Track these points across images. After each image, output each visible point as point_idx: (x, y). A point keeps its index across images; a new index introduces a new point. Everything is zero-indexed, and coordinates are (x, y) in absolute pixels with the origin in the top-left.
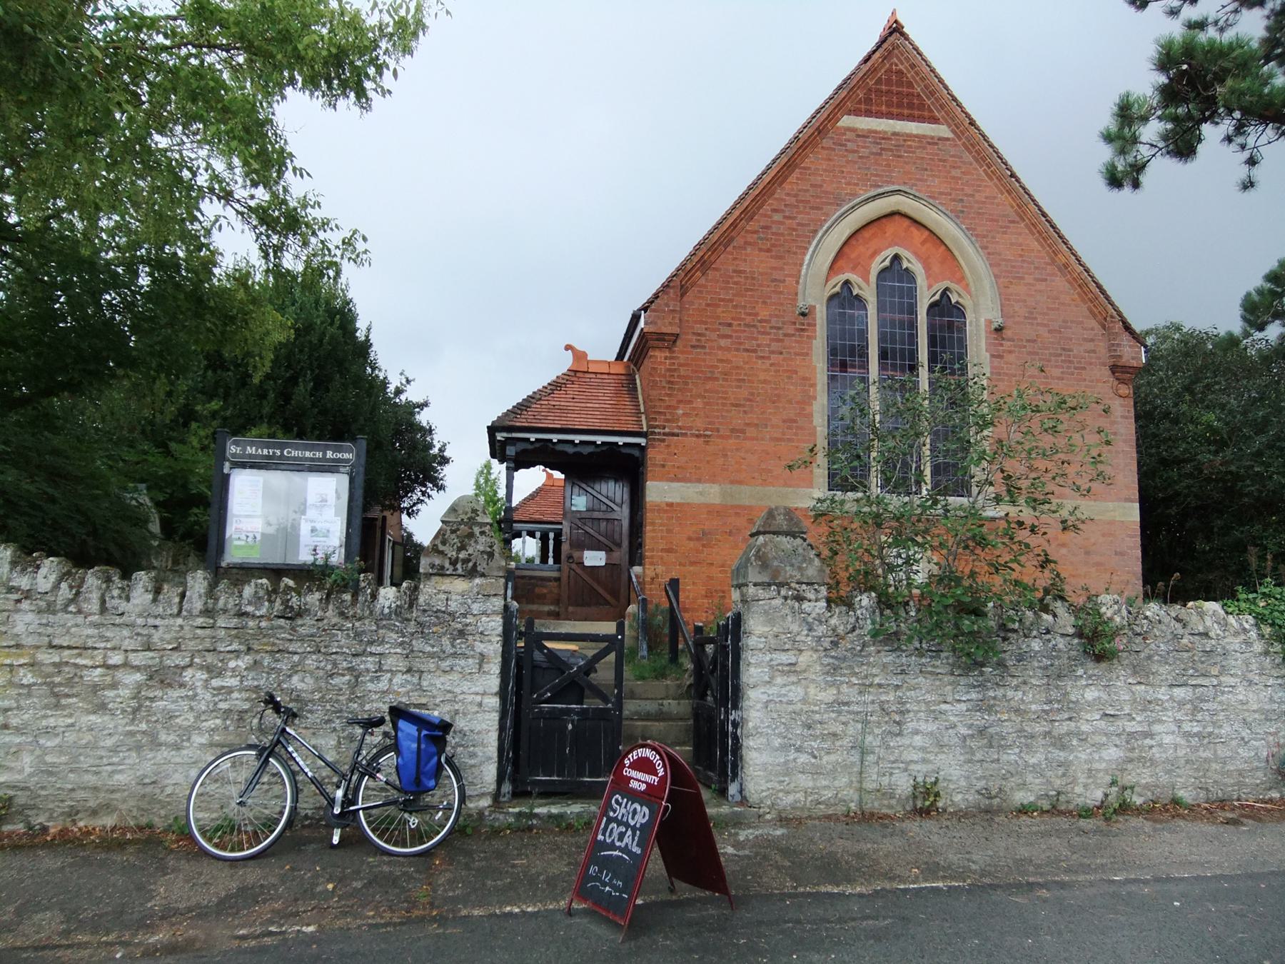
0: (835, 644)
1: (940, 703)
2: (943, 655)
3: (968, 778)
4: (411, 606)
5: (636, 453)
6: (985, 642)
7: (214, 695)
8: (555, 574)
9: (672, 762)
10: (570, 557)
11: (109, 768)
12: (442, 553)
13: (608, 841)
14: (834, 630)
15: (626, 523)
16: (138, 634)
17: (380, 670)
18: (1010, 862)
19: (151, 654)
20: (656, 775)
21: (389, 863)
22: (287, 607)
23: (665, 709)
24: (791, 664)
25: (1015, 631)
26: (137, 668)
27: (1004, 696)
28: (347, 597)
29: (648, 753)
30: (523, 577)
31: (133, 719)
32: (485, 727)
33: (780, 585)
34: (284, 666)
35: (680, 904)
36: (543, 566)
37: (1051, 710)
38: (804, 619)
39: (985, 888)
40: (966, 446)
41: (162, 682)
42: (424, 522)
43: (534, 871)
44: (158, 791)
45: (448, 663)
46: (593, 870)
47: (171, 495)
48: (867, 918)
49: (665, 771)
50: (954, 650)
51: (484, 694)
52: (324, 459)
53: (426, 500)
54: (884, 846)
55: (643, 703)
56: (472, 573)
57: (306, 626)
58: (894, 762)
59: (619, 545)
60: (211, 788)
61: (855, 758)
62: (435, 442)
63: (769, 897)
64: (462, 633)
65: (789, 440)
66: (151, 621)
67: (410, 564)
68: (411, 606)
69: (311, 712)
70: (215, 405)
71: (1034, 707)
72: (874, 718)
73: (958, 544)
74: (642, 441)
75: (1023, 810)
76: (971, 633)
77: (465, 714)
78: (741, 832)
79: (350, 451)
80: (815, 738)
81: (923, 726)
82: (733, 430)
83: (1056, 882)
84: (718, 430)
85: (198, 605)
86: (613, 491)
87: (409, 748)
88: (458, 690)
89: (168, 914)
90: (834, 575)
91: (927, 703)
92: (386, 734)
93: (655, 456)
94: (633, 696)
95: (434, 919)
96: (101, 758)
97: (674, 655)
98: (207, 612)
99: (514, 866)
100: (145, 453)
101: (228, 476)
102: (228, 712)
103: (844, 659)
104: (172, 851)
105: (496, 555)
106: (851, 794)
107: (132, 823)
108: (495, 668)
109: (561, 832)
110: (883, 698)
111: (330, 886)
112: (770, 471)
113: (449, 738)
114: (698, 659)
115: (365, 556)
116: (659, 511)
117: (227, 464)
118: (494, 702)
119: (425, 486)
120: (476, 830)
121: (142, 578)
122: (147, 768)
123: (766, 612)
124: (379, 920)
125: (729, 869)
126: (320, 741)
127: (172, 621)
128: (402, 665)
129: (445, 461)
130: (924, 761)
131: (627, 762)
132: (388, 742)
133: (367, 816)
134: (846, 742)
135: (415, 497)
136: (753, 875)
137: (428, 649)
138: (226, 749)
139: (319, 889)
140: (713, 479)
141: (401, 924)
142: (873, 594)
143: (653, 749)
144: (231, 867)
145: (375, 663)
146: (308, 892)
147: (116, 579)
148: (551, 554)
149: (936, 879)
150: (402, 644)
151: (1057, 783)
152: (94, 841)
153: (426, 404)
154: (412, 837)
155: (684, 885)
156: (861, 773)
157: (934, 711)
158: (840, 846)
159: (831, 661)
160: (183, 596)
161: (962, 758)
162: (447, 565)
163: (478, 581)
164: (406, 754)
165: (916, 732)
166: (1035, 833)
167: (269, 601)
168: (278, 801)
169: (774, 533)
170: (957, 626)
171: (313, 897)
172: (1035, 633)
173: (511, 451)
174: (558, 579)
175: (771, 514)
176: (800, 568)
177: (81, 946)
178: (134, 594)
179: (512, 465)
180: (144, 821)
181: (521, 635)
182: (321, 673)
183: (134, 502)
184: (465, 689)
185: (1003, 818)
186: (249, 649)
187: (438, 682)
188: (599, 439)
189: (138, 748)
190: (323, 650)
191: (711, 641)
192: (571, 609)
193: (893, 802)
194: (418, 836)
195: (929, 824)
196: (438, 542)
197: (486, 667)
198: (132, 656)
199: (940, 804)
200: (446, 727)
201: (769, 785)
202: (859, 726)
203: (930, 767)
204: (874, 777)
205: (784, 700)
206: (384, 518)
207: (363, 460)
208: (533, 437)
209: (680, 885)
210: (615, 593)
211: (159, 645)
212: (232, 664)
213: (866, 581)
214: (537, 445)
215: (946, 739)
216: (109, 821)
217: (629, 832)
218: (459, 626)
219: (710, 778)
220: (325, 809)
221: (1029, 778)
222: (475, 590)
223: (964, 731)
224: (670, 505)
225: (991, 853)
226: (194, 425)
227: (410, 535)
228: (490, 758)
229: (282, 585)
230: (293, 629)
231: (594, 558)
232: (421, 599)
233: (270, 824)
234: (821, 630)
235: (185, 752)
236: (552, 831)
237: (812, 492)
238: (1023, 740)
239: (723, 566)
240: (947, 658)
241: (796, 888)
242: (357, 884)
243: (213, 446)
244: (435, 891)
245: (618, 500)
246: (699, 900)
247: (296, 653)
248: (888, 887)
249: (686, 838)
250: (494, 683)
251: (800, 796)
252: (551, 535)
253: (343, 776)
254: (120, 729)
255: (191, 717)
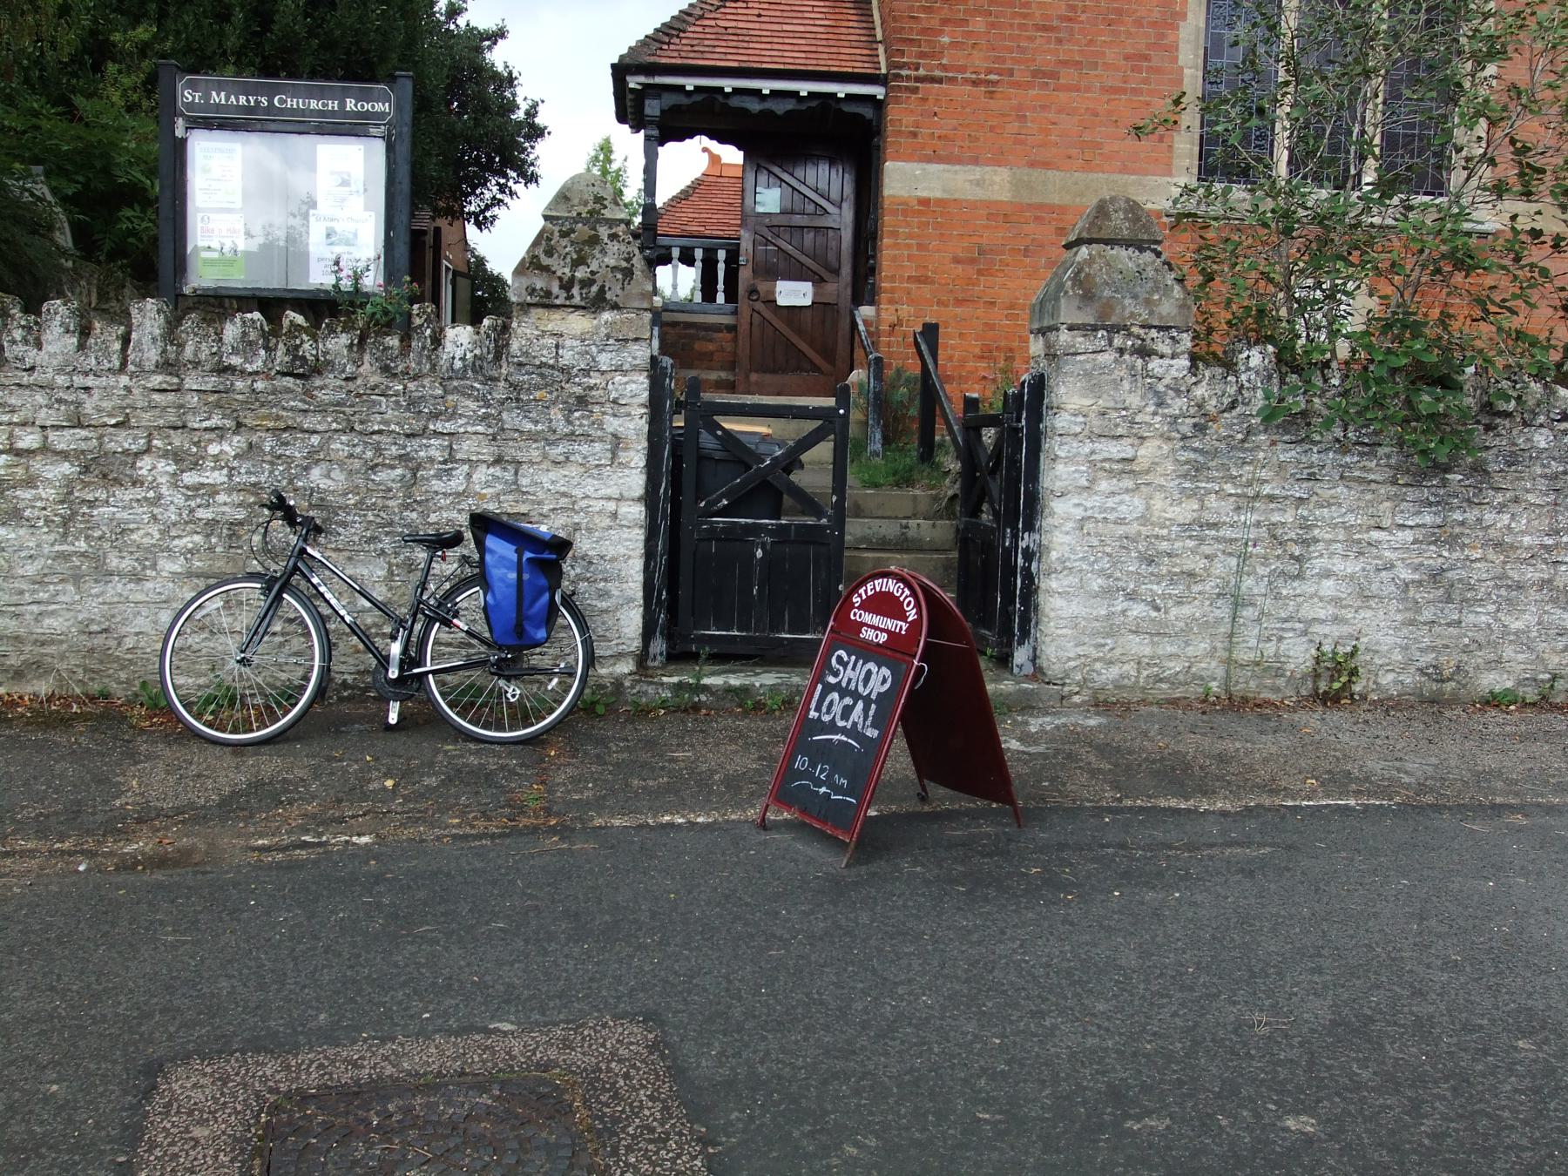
0: (1200, 429)
1: (1369, 528)
2: (1381, 451)
3: (1406, 648)
4: (498, 357)
5: (868, 112)
6: (1455, 432)
7: (188, 498)
8: (727, 320)
9: (932, 601)
10: (753, 291)
11: (35, 608)
12: (546, 269)
13: (826, 718)
14: (1200, 406)
15: (847, 236)
16: (59, 401)
17: (451, 458)
18: (1467, 776)
19: (84, 433)
20: (904, 618)
21: (477, 752)
22: (296, 357)
23: (911, 533)
24: (1124, 460)
25: (1507, 415)
26: (64, 455)
27: (1479, 520)
28: (393, 342)
29: (891, 586)
30: (675, 324)
31: (65, 535)
32: (622, 551)
33: (1113, 329)
34: (296, 452)
35: (935, 817)
36: (708, 306)
37: (1557, 545)
38: (1151, 387)
39: (1420, 809)
40: (1451, 93)
41: (105, 476)
42: (505, 237)
43: (704, 767)
44: (113, 643)
45: (560, 449)
46: (801, 762)
47: (86, 185)
48: (1231, 844)
49: (919, 613)
50: (1401, 443)
51: (620, 499)
52: (342, 112)
53: (507, 199)
54: (1261, 746)
55: (875, 523)
56: (597, 303)
57: (328, 388)
58: (1286, 620)
59: (836, 272)
60: (194, 640)
61: (1223, 611)
62: (519, 100)
63: (1073, 813)
64: (582, 402)
65: (1135, 91)
66: (79, 380)
67: (483, 297)
68: (498, 357)
69: (344, 524)
70: (143, 32)
71: (1527, 540)
72: (1259, 550)
73: (1424, 267)
74: (878, 91)
75: (1493, 701)
76: (1432, 416)
77: (588, 529)
78: (1032, 721)
79: (386, 99)
80: (1159, 578)
81: (1339, 565)
82: (1035, 74)
83: (1539, 805)
84: (1011, 73)
85: (152, 355)
86: (827, 181)
87: (502, 580)
88: (578, 492)
89: (146, 817)
90: (1206, 316)
91: (1348, 528)
92: (465, 560)
93: (900, 116)
94: (858, 512)
95: (552, 831)
96: (21, 592)
97: (928, 450)
98: (167, 366)
99: (673, 760)
100: (36, 114)
101: (184, 141)
102: (212, 524)
103: (1215, 453)
104: (142, 731)
105: (637, 273)
106: (1213, 668)
107: (78, 691)
108: (637, 458)
109: (745, 714)
110: (1276, 518)
111: (389, 783)
112: (1099, 146)
113: (566, 567)
114: (969, 452)
115: (416, 272)
116: (905, 213)
117: (180, 122)
118: (637, 512)
119: (505, 176)
120: (611, 709)
121: (58, 311)
122: (92, 609)
123: (1088, 375)
124: (468, 830)
125: (1015, 769)
126: (361, 571)
127: (112, 380)
128: (487, 452)
129: (537, 133)
130: (1336, 620)
131: (856, 599)
132: (468, 571)
133: (439, 683)
134: (1209, 586)
135: (488, 195)
136: (1052, 780)
137: (529, 426)
138: (212, 581)
139: (374, 786)
140: (998, 160)
141: (501, 836)
142: (1270, 348)
143: (900, 579)
144: (234, 754)
145: (443, 448)
146: (357, 791)
147: (16, 311)
148: (721, 286)
149: (1344, 793)
150: (485, 417)
151: (1554, 660)
152: (23, 715)
153: (500, 34)
154: (512, 717)
155: (942, 791)
156: (1231, 635)
157: (1359, 541)
158: (1192, 745)
159: (1192, 456)
160: (126, 340)
161: (1399, 617)
162: (555, 289)
163: (607, 316)
164: (498, 586)
165: (1327, 574)
166: (1512, 735)
167: (267, 348)
168: (297, 659)
169: (1106, 242)
170: (1408, 403)
171: (365, 797)
172: (1542, 419)
173: (653, 108)
174: (732, 329)
175: (1102, 210)
176: (1148, 302)
177: (23, 854)
178: (47, 337)
179: (655, 133)
180: (95, 687)
181: (679, 407)
182: (357, 464)
183: (27, 198)
184: (590, 490)
185: (1459, 711)
186: (239, 425)
187: (545, 479)
188: (804, 88)
189: (77, 579)
190: (357, 427)
191: (992, 421)
192: (754, 377)
193: (1281, 682)
194: (522, 715)
195: (1334, 717)
196: (540, 251)
197: (623, 456)
198: (53, 436)
199: (1357, 688)
200: (561, 546)
201: (1080, 651)
202: (1233, 562)
203: (1346, 630)
204: (1253, 642)
205: (1111, 517)
206: (438, 231)
207: (408, 117)
208: (690, 83)
209: (938, 791)
210: (829, 354)
211: (95, 418)
212: (213, 449)
213: (1258, 326)
214: (698, 98)
215: (1374, 587)
216: (43, 687)
217: (860, 705)
218: (578, 390)
219: (983, 637)
220: (374, 673)
221: (1508, 652)
222: (603, 331)
223: (1406, 574)
224: (925, 202)
225: (1434, 760)
226: (112, 68)
227: (481, 262)
228: (631, 600)
229: (286, 323)
230: (308, 393)
231: (794, 294)
232: (515, 346)
233: (290, 695)
234: (1177, 405)
235: (149, 585)
236: (731, 712)
237: (1168, 184)
238: (1503, 592)
239: (1012, 307)
240: (1388, 456)
241: (1120, 800)
242: (432, 781)
243: (145, 104)
244: (551, 791)
245: (835, 195)
246: (967, 813)
247: (315, 432)
248: (1267, 802)
249: (950, 721)
250: (635, 481)
251: (1130, 668)
252: (722, 255)
253: (401, 623)
254: (46, 549)
255: (154, 530)
